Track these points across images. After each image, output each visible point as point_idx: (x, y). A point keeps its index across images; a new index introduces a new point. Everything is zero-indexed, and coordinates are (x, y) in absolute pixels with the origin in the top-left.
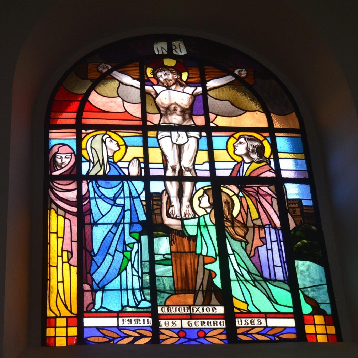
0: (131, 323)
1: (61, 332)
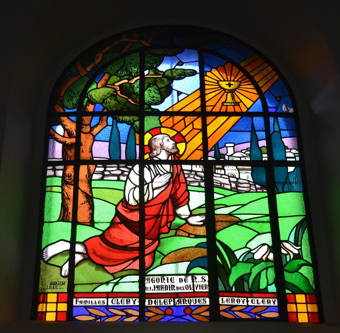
0: (82, 304)
1: (51, 307)
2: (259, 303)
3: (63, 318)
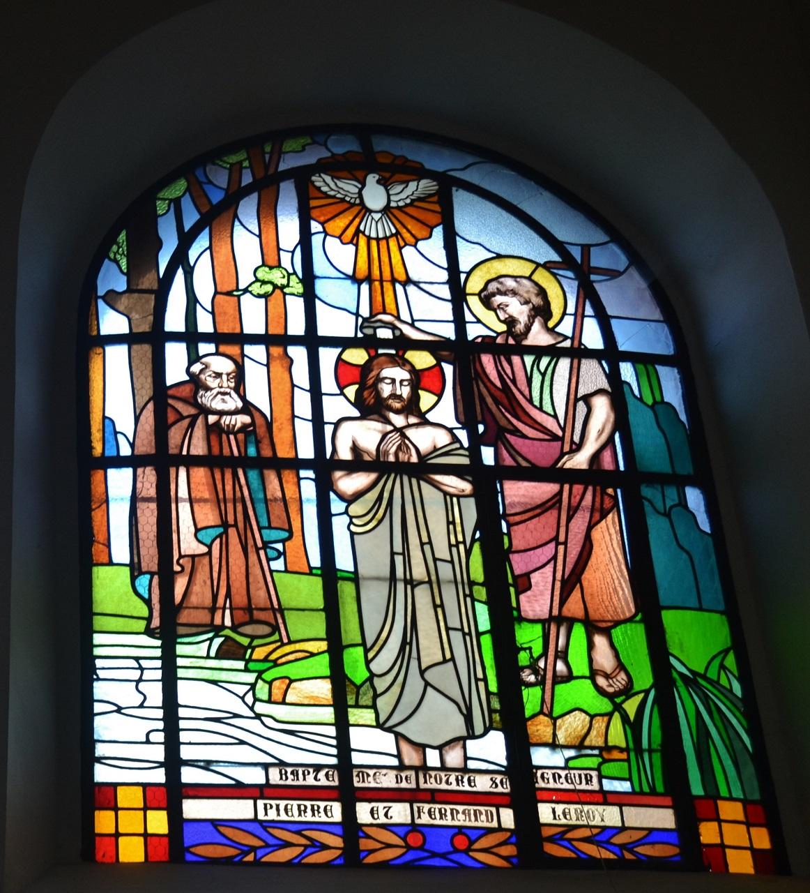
3: (162, 853)
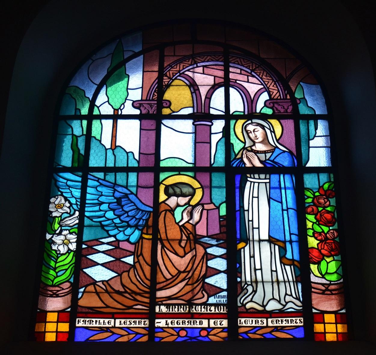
1: (51, 327)
2: (241, 323)
3: (65, 339)
